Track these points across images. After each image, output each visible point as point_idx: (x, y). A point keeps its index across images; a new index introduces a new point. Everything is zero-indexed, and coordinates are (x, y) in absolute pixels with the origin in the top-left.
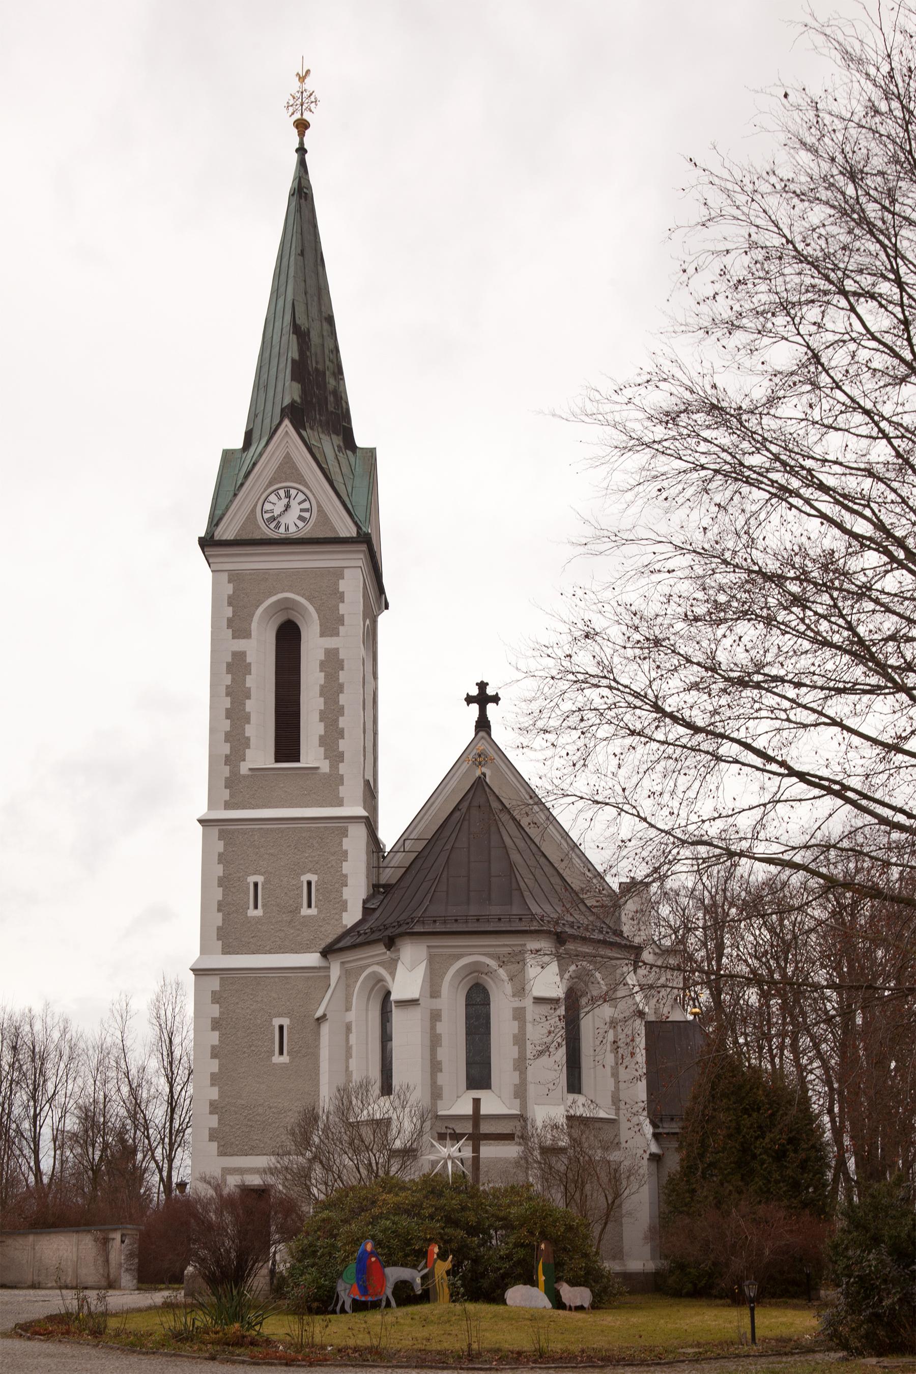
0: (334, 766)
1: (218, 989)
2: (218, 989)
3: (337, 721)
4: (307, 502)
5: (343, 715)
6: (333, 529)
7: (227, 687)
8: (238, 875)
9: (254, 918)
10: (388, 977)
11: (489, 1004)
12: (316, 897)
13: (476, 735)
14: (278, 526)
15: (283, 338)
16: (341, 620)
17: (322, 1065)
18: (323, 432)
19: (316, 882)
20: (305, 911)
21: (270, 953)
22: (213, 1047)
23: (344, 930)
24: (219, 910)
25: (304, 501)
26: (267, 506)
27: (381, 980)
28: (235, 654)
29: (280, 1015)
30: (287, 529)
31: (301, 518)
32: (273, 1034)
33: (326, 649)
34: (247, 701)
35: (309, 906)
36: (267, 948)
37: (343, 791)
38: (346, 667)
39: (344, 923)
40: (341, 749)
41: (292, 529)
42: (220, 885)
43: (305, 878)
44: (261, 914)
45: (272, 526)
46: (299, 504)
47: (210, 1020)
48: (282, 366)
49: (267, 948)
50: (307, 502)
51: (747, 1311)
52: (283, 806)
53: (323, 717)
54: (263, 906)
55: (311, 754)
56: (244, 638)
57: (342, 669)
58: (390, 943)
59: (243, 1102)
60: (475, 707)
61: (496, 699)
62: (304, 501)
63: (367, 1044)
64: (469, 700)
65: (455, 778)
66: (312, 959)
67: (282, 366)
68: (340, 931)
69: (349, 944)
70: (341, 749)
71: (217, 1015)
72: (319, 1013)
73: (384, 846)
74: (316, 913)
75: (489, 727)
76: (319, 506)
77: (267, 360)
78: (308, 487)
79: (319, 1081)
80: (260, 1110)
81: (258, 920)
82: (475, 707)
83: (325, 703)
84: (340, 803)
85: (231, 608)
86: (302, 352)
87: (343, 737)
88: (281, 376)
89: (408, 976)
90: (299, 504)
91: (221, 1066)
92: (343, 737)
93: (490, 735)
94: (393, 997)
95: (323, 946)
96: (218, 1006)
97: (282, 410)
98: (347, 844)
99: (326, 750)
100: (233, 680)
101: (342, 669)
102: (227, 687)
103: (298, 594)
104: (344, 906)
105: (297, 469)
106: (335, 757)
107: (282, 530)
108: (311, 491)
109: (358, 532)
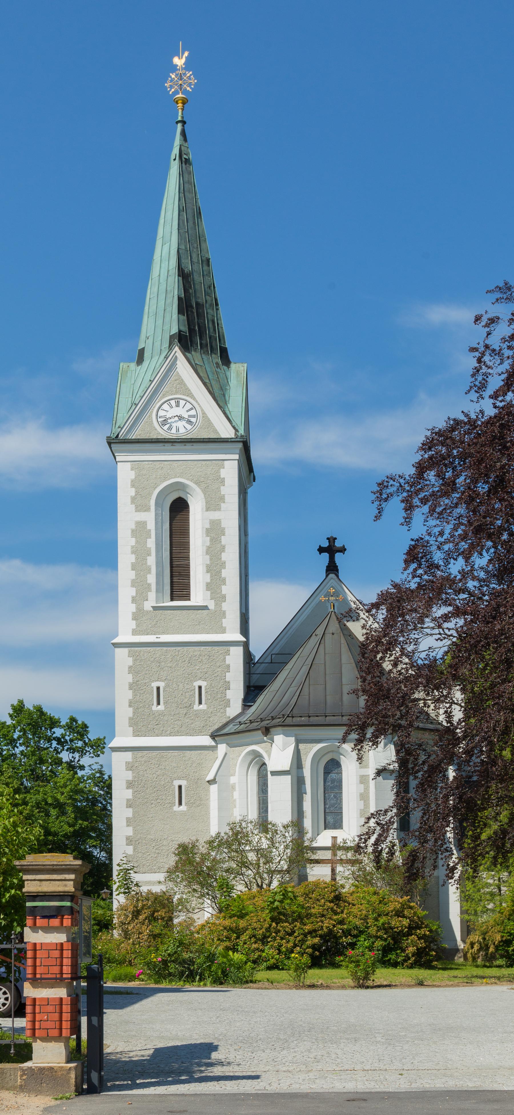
0: (218, 604)
1: (131, 760)
2: (131, 760)
3: (220, 572)
4: (194, 410)
5: (225, 568)
6: (216, 431)
7: (132, 547)
8: (145, 681)
9: (157, 711)
10: (265, 755)
11: (341, 773)
12: (206, 696)
13: (327, 576)
14: (170, 428)
15: (170, 279)
16: (222, 499)
17: (211, 812)
18: (204, 353)
19: (206, 687)
20: (196, 707)
21: (171, 736)
22: (128, 800)
23: (228, 720)
24: (130, 706)
25: (192, 409)
26: (161, 413)
27: (257, 755)
28: (138, 523)
29: (179, 778)
30: (178, 430)
31: (178, 405)
32: (174, 790)
33: (210, 520)
34: (148, 557)
35: (200, 703)
36: (168, 732)
37: (225, 622)
38: (226, 534)
39: (228, 715)
40: (223, 593)
41: (182, 430)
42: (130, 689)
43: (197, 684)
44: (163, 709)
45: (166, 427)
46: (188, 411)
47: (125, 782)
48: (169, 301)
49: (168, 732)
50: (194, 410)
51: (287, 767)
52: (178, 633)
53: (209, 569)
54: (164, 703)
55: (198, 595)
56: (145, 511)
57: (224, 535)
58: (267, 731)
59: (152, 837)
60: (326, 556)
61: (343, 550)
62: (192, 409)
63: (247, 798)
64: (321, 550)
65: (309, 609)
66: (206, 741)
67: (169, 301)
68: (225, 720)
69: (232, 731)
70: (223, 593)
71: (130, 778)
72: (210, 777)
73: (254, 657)
74: (205, 708)
75: (337, 570)
76: (204, 413)
77: (156, 295)
78: (194, 399)
79: (209, 823)
80: (165, 843)
81: (161, 714)
82: (326, 556)
83: (211, 559)
84: (223, 631)
85: (134, 489)
86: (186, 291)
87: (225, 584)
88: (168, 309)
89: (280, 751)
90: (188, 411)
91: (134, 813)
92: (225, 584)
93: (338, 576)
94: (270, 768)
95: (211, 731)
96: (131, 772)
97: (171, 337)
98: (229, 660)
99: (211, 593)
100: (137, 542)
101: (224, 535)
102: (132, 547)
103: (188, 479)
104: (227, 703)
105: (185, 385)
106: (220, 598)
107: (174, 431)
108: (197, 402)
109: (236, 434)
